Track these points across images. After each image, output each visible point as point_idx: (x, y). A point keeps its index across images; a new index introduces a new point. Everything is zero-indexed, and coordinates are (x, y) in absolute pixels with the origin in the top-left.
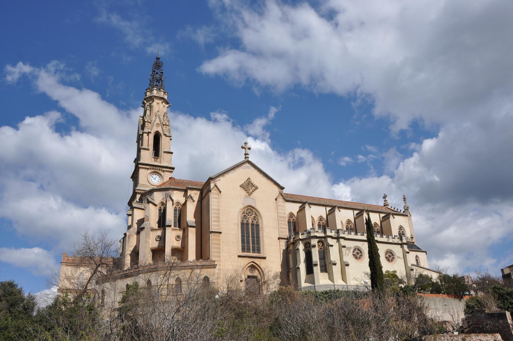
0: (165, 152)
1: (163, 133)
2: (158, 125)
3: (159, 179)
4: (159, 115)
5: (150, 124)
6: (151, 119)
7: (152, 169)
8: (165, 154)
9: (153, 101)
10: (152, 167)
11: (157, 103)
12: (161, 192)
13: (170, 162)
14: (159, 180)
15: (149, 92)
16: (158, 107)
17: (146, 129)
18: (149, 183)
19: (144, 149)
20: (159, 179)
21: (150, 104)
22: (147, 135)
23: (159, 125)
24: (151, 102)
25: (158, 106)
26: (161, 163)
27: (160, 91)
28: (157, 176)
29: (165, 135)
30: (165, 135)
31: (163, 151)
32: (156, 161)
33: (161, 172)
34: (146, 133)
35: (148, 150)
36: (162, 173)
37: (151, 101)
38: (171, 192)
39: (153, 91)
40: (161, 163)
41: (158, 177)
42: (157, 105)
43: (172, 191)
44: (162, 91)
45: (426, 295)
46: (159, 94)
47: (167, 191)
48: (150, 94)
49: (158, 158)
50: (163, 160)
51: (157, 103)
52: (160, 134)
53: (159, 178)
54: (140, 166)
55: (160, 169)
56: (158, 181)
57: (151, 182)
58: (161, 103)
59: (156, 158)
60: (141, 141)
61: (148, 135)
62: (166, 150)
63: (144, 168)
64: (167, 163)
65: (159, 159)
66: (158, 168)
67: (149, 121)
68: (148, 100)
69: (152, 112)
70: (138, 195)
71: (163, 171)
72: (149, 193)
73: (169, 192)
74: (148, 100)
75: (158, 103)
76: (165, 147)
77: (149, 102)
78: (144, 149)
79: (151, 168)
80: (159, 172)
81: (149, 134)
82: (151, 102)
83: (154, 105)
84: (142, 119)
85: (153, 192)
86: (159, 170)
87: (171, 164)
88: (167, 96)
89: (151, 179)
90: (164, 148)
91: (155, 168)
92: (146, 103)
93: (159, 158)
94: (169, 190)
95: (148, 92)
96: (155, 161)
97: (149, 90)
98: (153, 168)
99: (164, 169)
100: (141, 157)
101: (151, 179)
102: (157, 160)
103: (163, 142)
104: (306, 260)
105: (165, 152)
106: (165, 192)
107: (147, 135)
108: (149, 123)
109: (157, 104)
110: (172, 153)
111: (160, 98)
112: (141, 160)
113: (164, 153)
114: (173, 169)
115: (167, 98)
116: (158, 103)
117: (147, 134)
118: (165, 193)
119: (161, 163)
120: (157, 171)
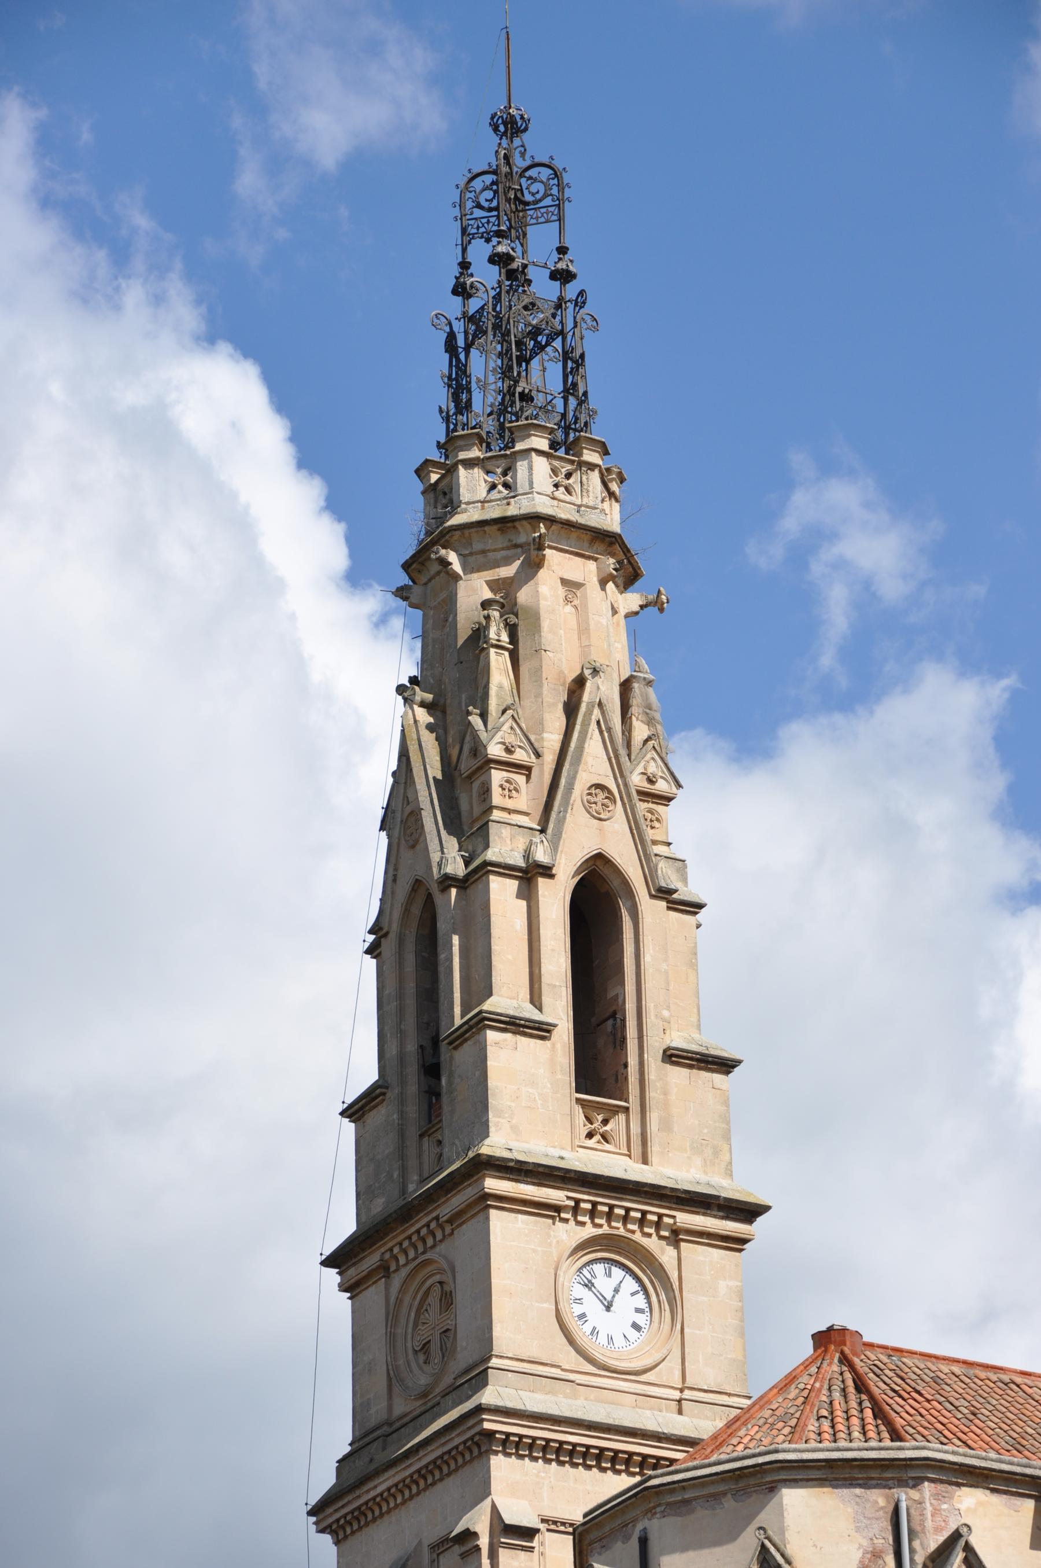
0: (672, 1057)
1: (650, 874)
2: (601, 796)
3: (638, 1310)
4: (600, 704)
5: (528, 777)
6: (532, 738)
7: (585, 1212)
8: (678, 1075)
9: (533, 566)
10: (604, 1202)
11: (564, 582)
12: (845, 1492)
13: (716, 1152)
14: (642, 1320)
15: (477, 472)
16: (573, 623)
17: (506, 831)
18: (571, 1341)
19: (514, 1025)
20: (638, 1310)
21: (507, 590)
22: (519, 896)
23: (611, 797)
24: (508, 571)
25: (569, 608)
26: (645, 1162)
27: (581, 464)
28: (618, 1273)
29: (664, 894)
30: (664, 894)
31: (655, 1045)
32: (605, 1138)
33: (652, 1244)
34: (506, 870)
35: (542, 1031)
36: (666, 1255)
37: (507, 561)
38: (937, 1496)
39: (521, 467)
40: (645, 1162)
41: (631, 1285)
42: (567, 600)
43: (941, 1487)
44: (592, 466)
45: (655, 1521)
46: (568, 490)
47: (902, 1483)
48: (493, 487)
49: (615, 1110)
50: (666, 1125)
51: (564, 582)
52: (615, 883)
53: (640, 1301)
54: (493, 1184)
55: (653, 1211)
56: (636, 1326)
57: (582, 1332)
58: (595, 580)
59: (599, 1107)
60: (456, 940)
61: (527, 890)
62: (678, 1040)
63: (525, 1202)
64: (698, 1161)
65: (622, 1117)
66: (637, 1207)
67: (521, 756)
68: (477, 546)
69: (538, 671)
70: (501, 1456)
71: (676, 1237)
72: (722, 1488)
73: (914, 1494)
74: (477, 546)
75: (570, 585)
76: (668, 1008)
77: (497, 565)
78: (514, 1025)
79: (577, 1202)
80: (638, 1237)
81: (542, 881)
82: (508, 571)
83: (544, 605)
84: (430, 727)
85: (772, 1489)
86: (642, 1222)
87: (729, 1172)
88: (616, 506)
89: (579, 1301)
90: (666, 1013)
91: (611, 1207)
92: (456, 577)
93: (627, 1109)
94: (917, 1483)
95: (469, 464)
96: (590, 1135)
97: (475, 453)
98: (594, 1204)
99: (686, 1219)
100: (492, 1101)
101: (579, 1301)
102: (605, 1122)
103: (648, 958)
104: (523, 1538)
105: (672, 1057)
106: (878, 1498)
107: (519, 896)
108: (520, 779)
109: (561, 591)
110: (725, 1065)
111: (587, 537)
112: (492, 1129)
113: (669, 1067)
114: (749, 1212)
115: (623, 522)
116: (570, 585)
117: (514, 884)
118: (882, 1502)
119: (654, 1157)
120: (622, 1231)
